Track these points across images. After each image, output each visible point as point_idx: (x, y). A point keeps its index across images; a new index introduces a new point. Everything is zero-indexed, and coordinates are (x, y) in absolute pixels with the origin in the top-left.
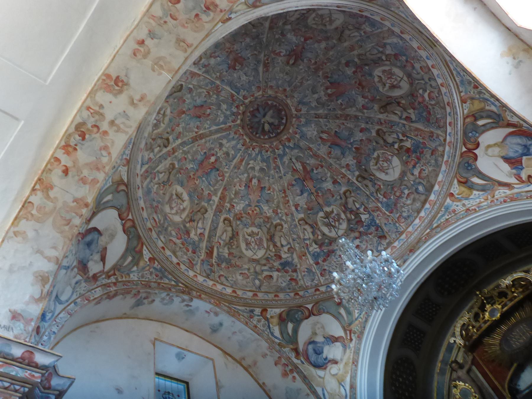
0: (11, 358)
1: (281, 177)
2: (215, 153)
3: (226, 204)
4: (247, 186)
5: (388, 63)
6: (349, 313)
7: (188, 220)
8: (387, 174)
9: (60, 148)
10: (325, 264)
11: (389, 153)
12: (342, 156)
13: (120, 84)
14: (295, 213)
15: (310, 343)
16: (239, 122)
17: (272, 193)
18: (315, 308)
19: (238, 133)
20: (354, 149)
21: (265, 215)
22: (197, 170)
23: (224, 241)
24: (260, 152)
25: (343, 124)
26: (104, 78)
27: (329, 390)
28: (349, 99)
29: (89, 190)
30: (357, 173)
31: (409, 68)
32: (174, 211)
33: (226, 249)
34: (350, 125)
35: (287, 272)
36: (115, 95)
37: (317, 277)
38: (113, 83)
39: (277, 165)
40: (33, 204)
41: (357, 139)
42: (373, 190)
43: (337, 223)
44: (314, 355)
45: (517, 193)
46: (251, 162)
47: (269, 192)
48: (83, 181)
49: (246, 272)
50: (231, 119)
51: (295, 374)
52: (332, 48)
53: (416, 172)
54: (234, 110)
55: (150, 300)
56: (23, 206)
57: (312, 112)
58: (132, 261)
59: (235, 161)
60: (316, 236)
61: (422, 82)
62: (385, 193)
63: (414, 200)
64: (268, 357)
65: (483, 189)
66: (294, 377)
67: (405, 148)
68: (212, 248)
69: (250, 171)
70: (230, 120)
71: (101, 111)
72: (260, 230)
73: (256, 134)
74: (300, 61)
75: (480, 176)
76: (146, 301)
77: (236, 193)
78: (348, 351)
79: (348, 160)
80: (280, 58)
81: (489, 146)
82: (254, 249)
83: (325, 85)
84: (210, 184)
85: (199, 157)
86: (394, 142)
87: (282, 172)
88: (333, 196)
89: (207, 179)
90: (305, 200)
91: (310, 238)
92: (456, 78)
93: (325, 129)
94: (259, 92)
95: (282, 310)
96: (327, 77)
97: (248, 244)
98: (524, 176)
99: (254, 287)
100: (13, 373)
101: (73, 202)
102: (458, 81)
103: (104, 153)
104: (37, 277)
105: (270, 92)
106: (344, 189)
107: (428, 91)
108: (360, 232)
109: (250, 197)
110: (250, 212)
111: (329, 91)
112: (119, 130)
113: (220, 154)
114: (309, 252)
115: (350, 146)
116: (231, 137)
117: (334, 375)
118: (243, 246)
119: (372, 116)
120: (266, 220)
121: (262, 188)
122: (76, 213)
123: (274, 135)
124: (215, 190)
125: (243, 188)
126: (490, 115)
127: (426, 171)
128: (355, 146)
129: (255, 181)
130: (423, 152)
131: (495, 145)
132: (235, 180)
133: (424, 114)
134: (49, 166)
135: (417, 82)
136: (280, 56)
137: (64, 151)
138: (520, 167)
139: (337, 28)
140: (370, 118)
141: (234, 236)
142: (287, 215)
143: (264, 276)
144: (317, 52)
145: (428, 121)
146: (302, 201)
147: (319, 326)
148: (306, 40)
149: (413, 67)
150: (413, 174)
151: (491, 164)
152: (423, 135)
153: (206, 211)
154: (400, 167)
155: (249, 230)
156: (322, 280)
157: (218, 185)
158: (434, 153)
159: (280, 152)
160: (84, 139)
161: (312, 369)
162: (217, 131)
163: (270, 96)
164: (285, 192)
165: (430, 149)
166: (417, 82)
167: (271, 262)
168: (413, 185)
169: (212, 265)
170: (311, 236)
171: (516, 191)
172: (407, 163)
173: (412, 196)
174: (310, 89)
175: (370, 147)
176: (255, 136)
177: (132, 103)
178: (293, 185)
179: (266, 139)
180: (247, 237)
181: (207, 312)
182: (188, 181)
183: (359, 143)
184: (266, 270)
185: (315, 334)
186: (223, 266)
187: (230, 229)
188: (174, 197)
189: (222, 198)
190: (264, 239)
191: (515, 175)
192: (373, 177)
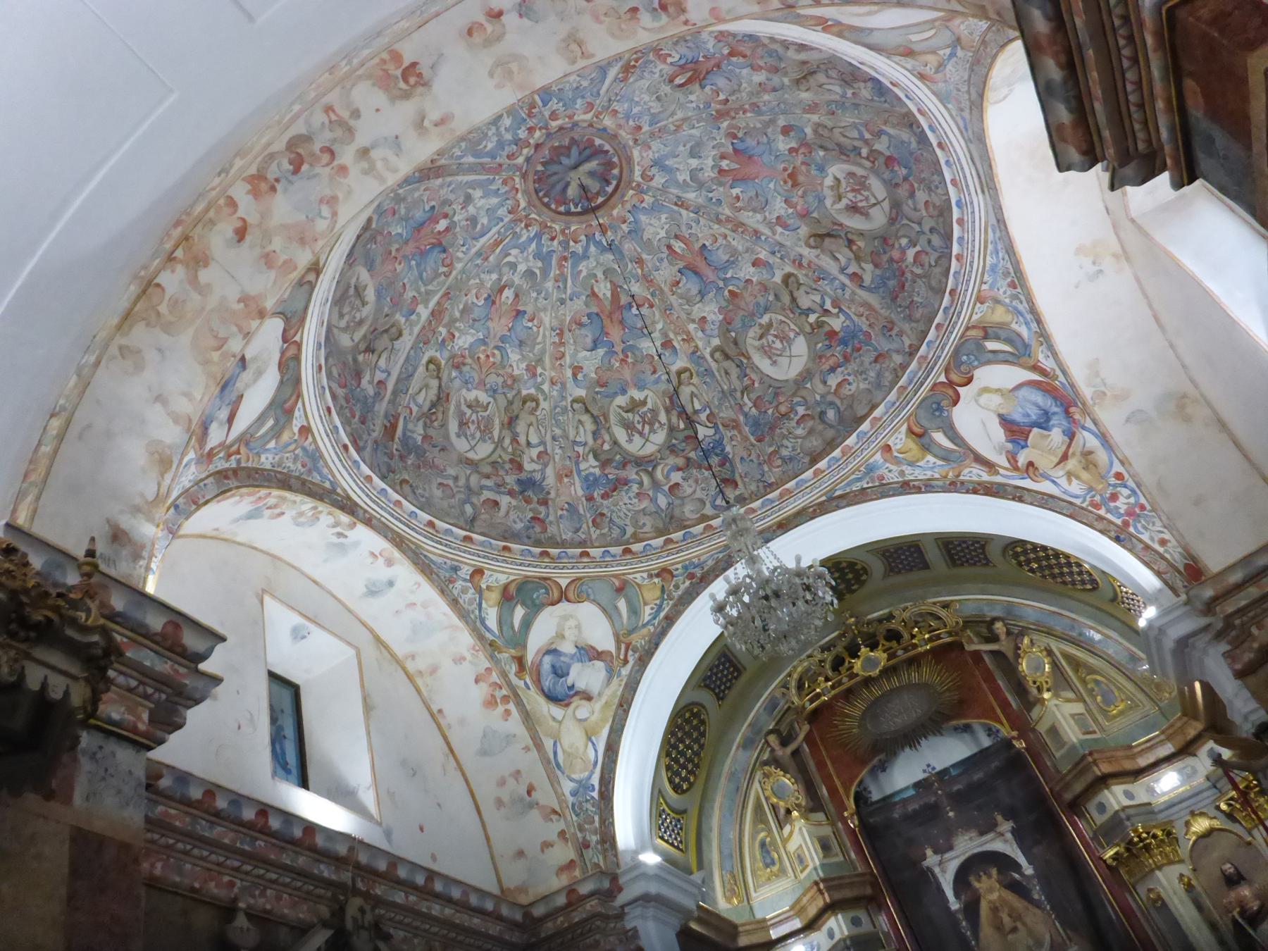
0: (143, 631)
1: (562, 302)
2: (451, 213)
3: (441, 329)
4: (491, 301)
5: (868, 164)
6: (634, 611)
7: (362, 347)
8: (775, 363)
9: (243, 180)
10: (605, 502)
11: (793, 326)
12: (698, 299)
13: (412, 80)
14: (570, 384)
15: (549, 652)
16: (521, 160)
17: (535, 329)
18: (572, 587)
19: (510, 183)
20: (726, 293)
21: (510, 370)
22: (406, 242)
23: (420, 407)
24: (538, 236)
25: (725, 237)
26: (385, 56)
27: (566, 746)
28: (757, 195)
29: (275, 282)
30: (716, 342)
31: (903, 192)
32: (343, 324)
33: (421, 423)
34: (738, 243)
35: (528, 501)
36: (393, 99)
37: (584, 526)
38: (399, 73)
39: (562, 274)
40: (163, 290)
41: (741, 275)
42: (737, 384)
43: (647, 427)
44: (552, 676)
45: (1000, 484)
46: (514, 252)
47: (530, 324)
48: (268, 260)
49: (451, 482)
50: (508, 150)
51: (511, 706)
52: (774, 90)
53: (833, 381)
54: (522, 134)
55: (277, 511)
56: (144, 292)
57: (674, 191)
58: (272, 428)
59: (483, 240)
60: (599, 442)
61: (917, 228)
62: (759, 397)
63: (811, 432)
64: (466, 664)
65: (946, 456)
66: (508, 712)
67: (827, 329)
68: (396, 418)
69: (505, 270)
70: (505, 153)
71: (352, 123)
72: (491, 400)
73: (545, 195)
74: (697, 85)
75: (950, 434)
76: (267, 513)
77: (466, 310)
78: (615, 681)
79: (707, 309)
80: (662, 66)
81: (986, 390)
82: (473, 436)
83: (722, 150)
84: (421, 277)
85: (419, 215)
86: (809, 309)
87: (569, 291)
88: (654, 372)
89: (418, 265)
90: (597, 362)
91: (585, 444)
92: (988, 258)
93: (685, 232)
94: (586, 113)
95: (512, 578)
96: (735, 137)
97: (463, 424)
98: (1022, 459)
99: (462, 519)
100: (148, 663)
101: (239, 301)
102: (988, 263)
103: (325, 211)
104: (152, 454)
105: (608, 122)
106: (680, 363)
107: (918, 248)
108: (688, 459)
109: (490, 324)
110: (482, 357)
111: (725, 164)
112: (370, 171)
113: (460, 217)
114: (579, 472)
115: (721, 284)
116: (493, 187)
117: (580, 720)
118: (453, 427)
119: (788, 243)
120: (509, 382)
121: (519, 314)
122: (240, 329)
123: (579, 209)
124: (428, 293)
125: (481, 302)
126: (1013, 339)
127: (853, 387)
128: (731, 288)
129: (508, 294)
130: (859, 350)
131: (998, 391)
132: (472, 282)
133: (892, 283)
134: (211, 214)
135: (905, 221)
136: (665, 62)
137: (249, 187)
138: (1023, 443)
139: (804, 63)
140: (782, 245)
141: (442, 398)
142: (553, 383)
143: (483, 498)
144: (740, 85)
145: (894, 299)
146: (591, 362)
147: (572, 623)
148: (731, 54)
149: (912, 194)
150: (825, 383)
151: (976, 420)
152: (872, 320)
153: (400, 335)
154: (805, 359)
155: (472, 395)
156: (595, 533)
157: (435, 283)
158: (881, 360)
159: (579, 249)
160: (296, 171)
161: (541, 700)
162: (472, 169)
163: (605, 129)
164: (561, 335)
165: (876, 350)
166: (905, 221)
167: (501, 473)
168: (818, 403)
169: (391, 456)
170: (591, 441)
171: (998, 479)
172: (820, 357)
173: (810, 423)
174: (688, 146)
175: (762, 301)
176: (540, 199)
177: (419, 124)
178: (581, 325)
179: (560, 213)
180: (464, 408)
181: (373, 554)
182: (383, 262)
183: (742, 284)
184: (488, 488)
185: (560, 636)
186: (409, 462)
187: (434, 383)
188: (352, 291)
189: (436, 314)
190: (497, 422)
191: (1008, 452)
192: (745, 361)
